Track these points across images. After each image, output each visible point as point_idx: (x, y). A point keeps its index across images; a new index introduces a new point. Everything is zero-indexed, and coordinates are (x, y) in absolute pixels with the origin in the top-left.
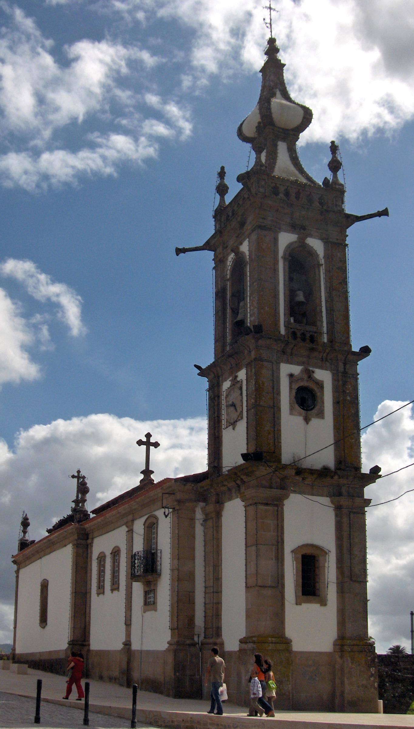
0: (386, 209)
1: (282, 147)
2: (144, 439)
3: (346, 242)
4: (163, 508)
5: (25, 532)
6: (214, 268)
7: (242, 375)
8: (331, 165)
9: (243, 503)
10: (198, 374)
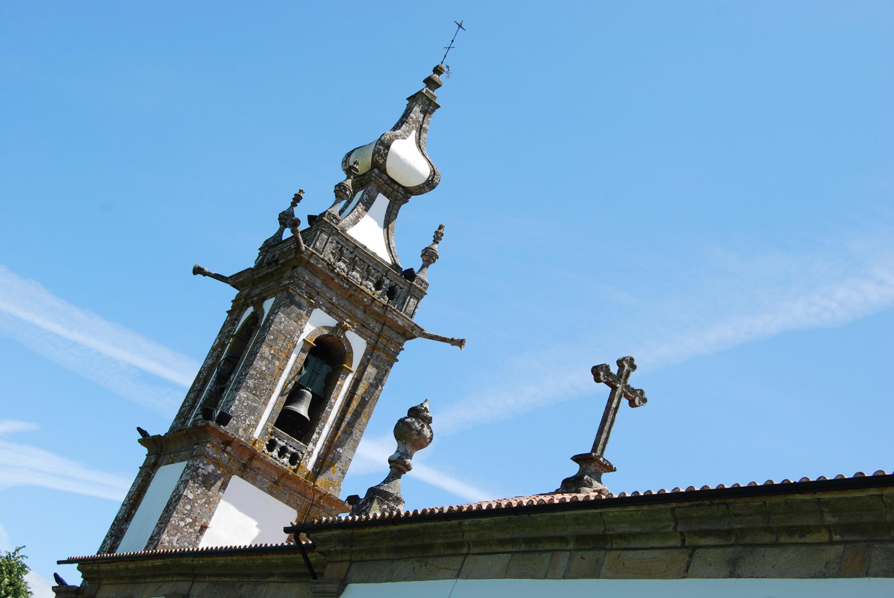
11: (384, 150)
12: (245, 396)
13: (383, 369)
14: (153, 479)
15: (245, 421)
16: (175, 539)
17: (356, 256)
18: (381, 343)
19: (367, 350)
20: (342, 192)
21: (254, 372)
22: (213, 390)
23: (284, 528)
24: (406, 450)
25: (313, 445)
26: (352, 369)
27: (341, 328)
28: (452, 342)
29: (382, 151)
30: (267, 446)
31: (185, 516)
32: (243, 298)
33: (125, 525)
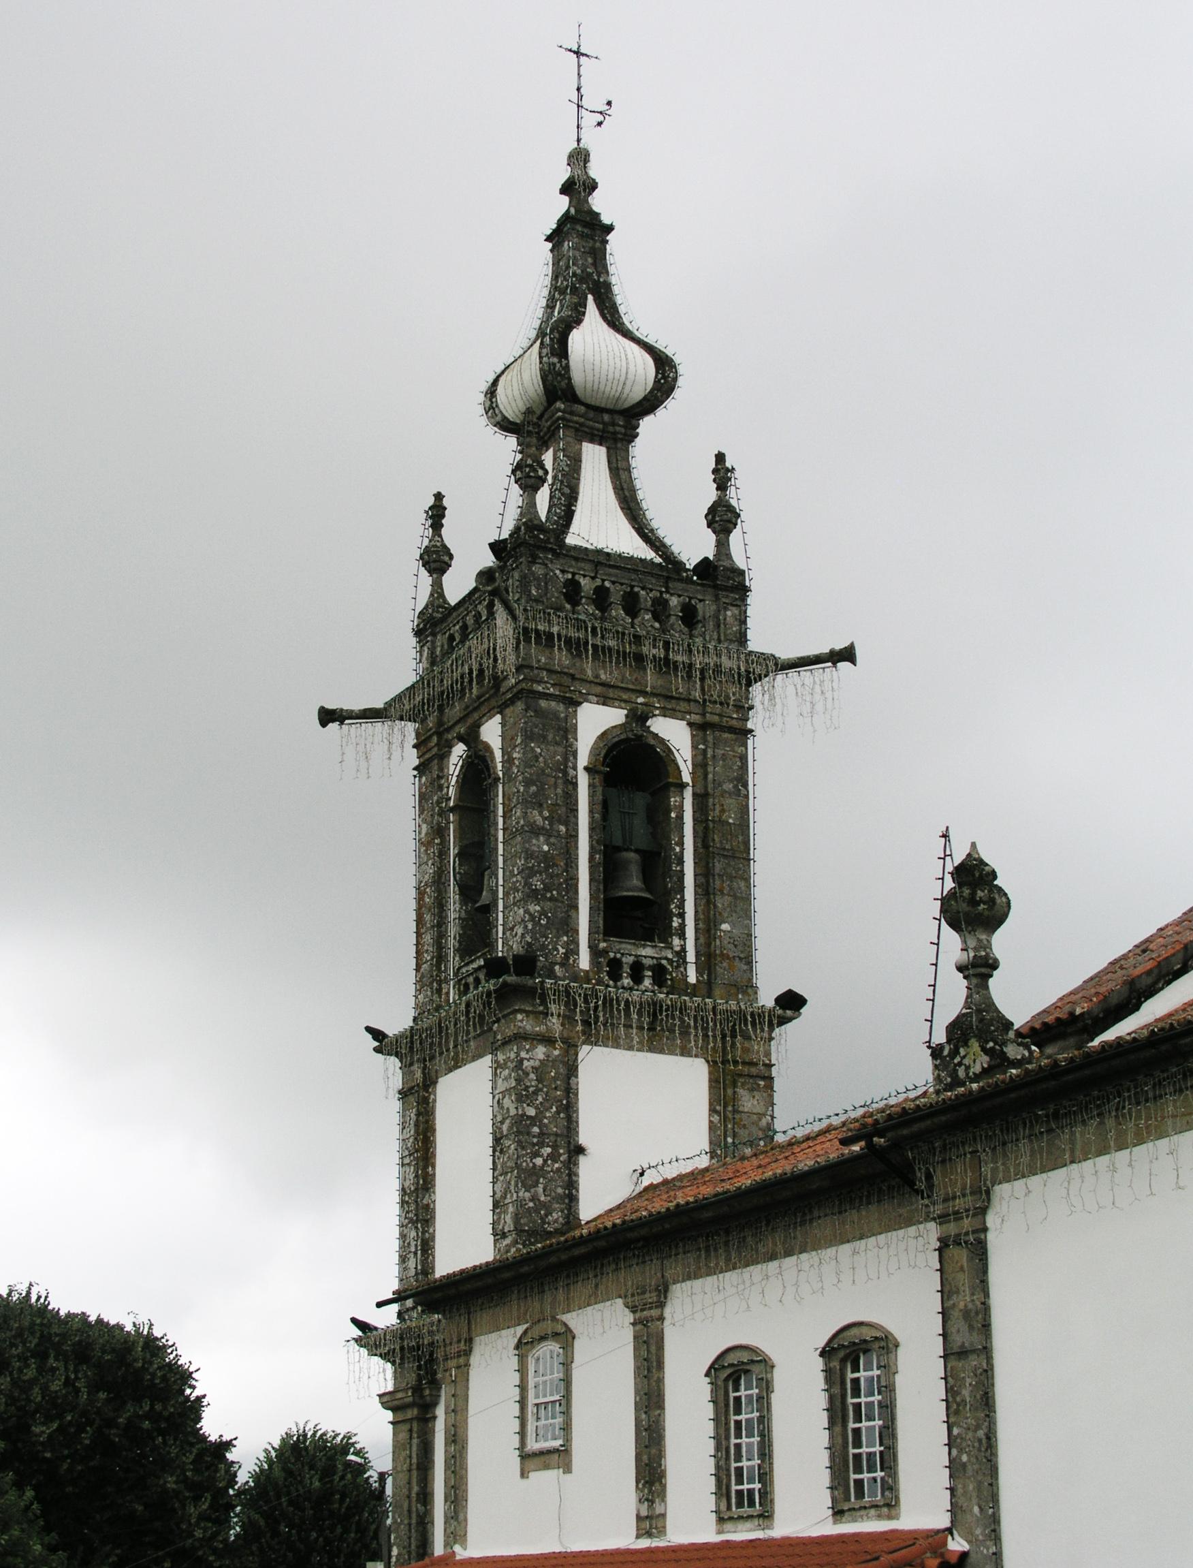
0: (324, 723)
1: (594, 457)
11: (560, 362)
12: (538, 908)
13: (734, 756)
14: (437, 1104)
15: (557, 950)
16: (540, 1189)
17: (603, 581)
18: (711, 713)
19: (693, 736)
20: (531, 477)
21: (533, 861)
22: (463, 915)
24: (979, 940)
25: (680, 939)
27: (639, 718)
29: (558, 365)
30: (609, 973)
31: (537, 1148)
32: (433, 734)
33: (427, 1196)
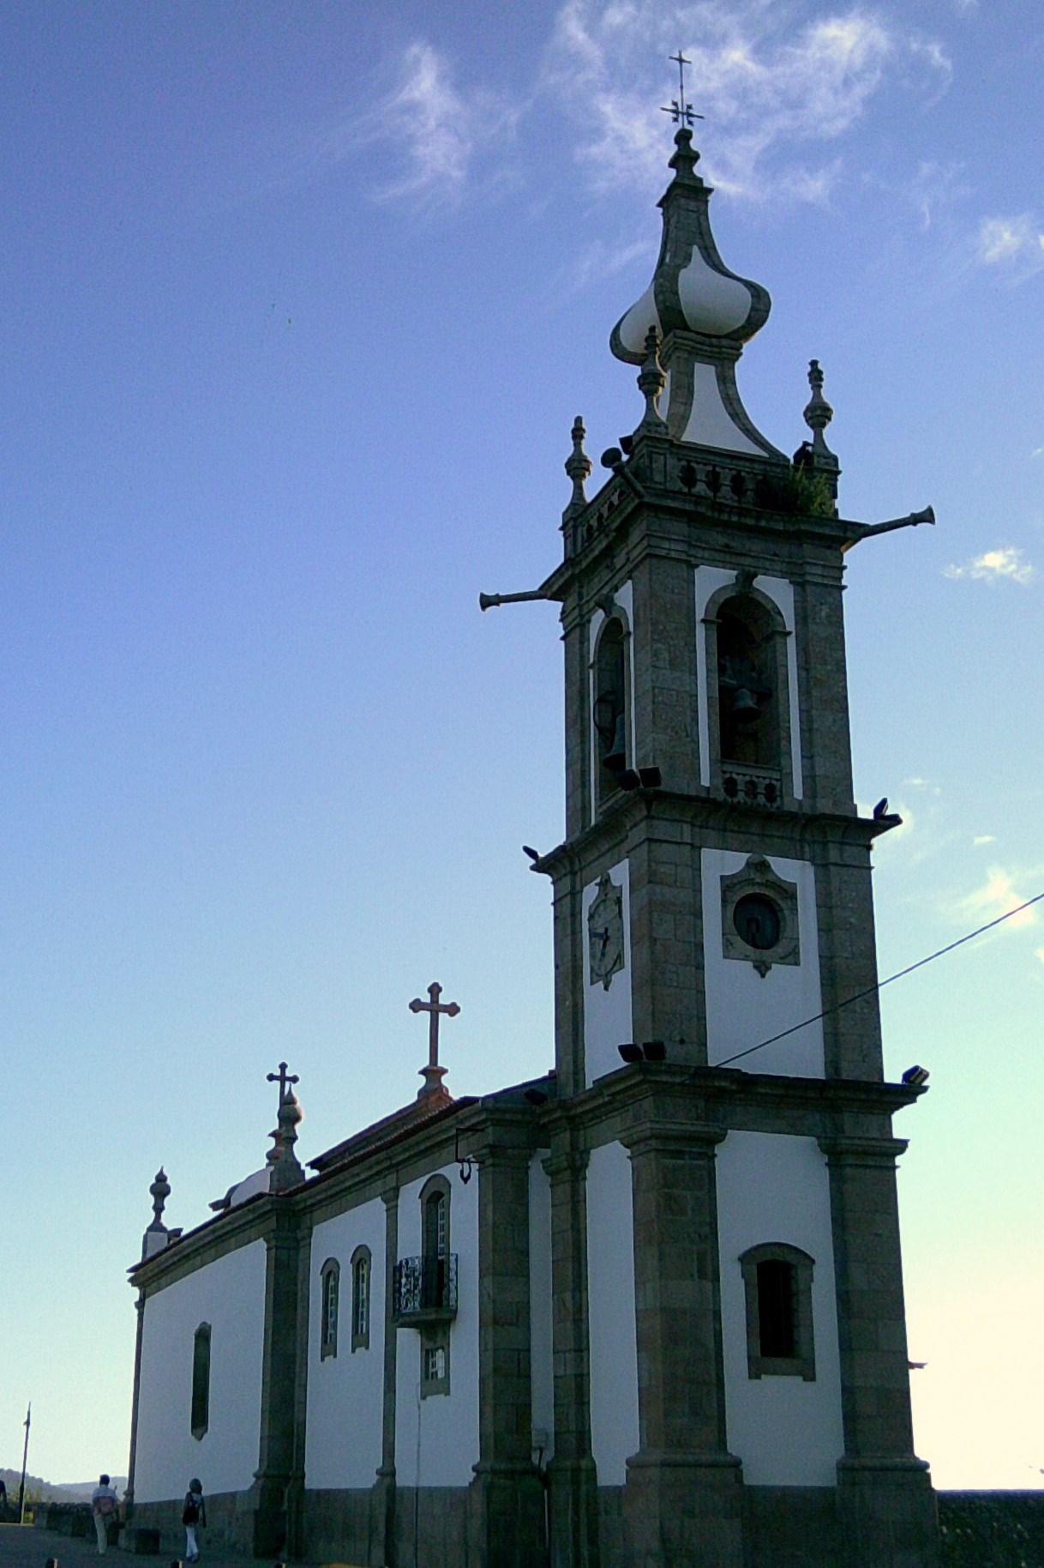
0: (930, 511)
1: (705, 375)
2: (426, 998)
3: (640, 373)
4: (458, 1161)
5: (159, 1209)
6: (563, 638)
7: (620, 874)
8: (809, 414)
9: (628, 1152)
10: (533, 868)
23: (750, 1377)
26: (788, 629)
27: (747, 578)
28: (915, 520)
